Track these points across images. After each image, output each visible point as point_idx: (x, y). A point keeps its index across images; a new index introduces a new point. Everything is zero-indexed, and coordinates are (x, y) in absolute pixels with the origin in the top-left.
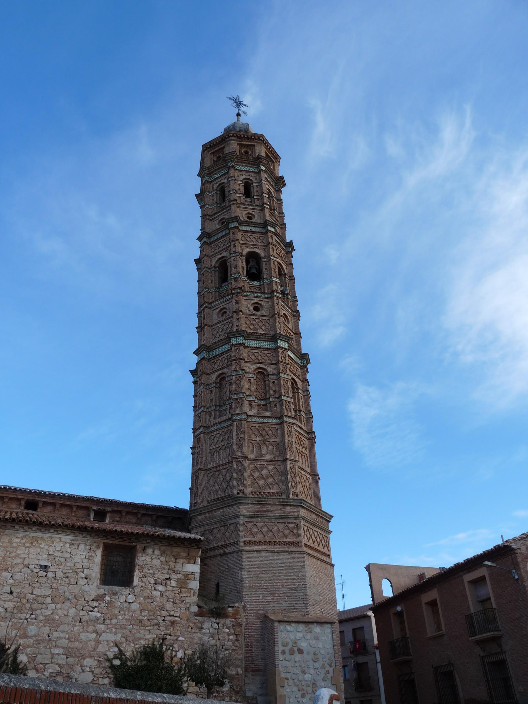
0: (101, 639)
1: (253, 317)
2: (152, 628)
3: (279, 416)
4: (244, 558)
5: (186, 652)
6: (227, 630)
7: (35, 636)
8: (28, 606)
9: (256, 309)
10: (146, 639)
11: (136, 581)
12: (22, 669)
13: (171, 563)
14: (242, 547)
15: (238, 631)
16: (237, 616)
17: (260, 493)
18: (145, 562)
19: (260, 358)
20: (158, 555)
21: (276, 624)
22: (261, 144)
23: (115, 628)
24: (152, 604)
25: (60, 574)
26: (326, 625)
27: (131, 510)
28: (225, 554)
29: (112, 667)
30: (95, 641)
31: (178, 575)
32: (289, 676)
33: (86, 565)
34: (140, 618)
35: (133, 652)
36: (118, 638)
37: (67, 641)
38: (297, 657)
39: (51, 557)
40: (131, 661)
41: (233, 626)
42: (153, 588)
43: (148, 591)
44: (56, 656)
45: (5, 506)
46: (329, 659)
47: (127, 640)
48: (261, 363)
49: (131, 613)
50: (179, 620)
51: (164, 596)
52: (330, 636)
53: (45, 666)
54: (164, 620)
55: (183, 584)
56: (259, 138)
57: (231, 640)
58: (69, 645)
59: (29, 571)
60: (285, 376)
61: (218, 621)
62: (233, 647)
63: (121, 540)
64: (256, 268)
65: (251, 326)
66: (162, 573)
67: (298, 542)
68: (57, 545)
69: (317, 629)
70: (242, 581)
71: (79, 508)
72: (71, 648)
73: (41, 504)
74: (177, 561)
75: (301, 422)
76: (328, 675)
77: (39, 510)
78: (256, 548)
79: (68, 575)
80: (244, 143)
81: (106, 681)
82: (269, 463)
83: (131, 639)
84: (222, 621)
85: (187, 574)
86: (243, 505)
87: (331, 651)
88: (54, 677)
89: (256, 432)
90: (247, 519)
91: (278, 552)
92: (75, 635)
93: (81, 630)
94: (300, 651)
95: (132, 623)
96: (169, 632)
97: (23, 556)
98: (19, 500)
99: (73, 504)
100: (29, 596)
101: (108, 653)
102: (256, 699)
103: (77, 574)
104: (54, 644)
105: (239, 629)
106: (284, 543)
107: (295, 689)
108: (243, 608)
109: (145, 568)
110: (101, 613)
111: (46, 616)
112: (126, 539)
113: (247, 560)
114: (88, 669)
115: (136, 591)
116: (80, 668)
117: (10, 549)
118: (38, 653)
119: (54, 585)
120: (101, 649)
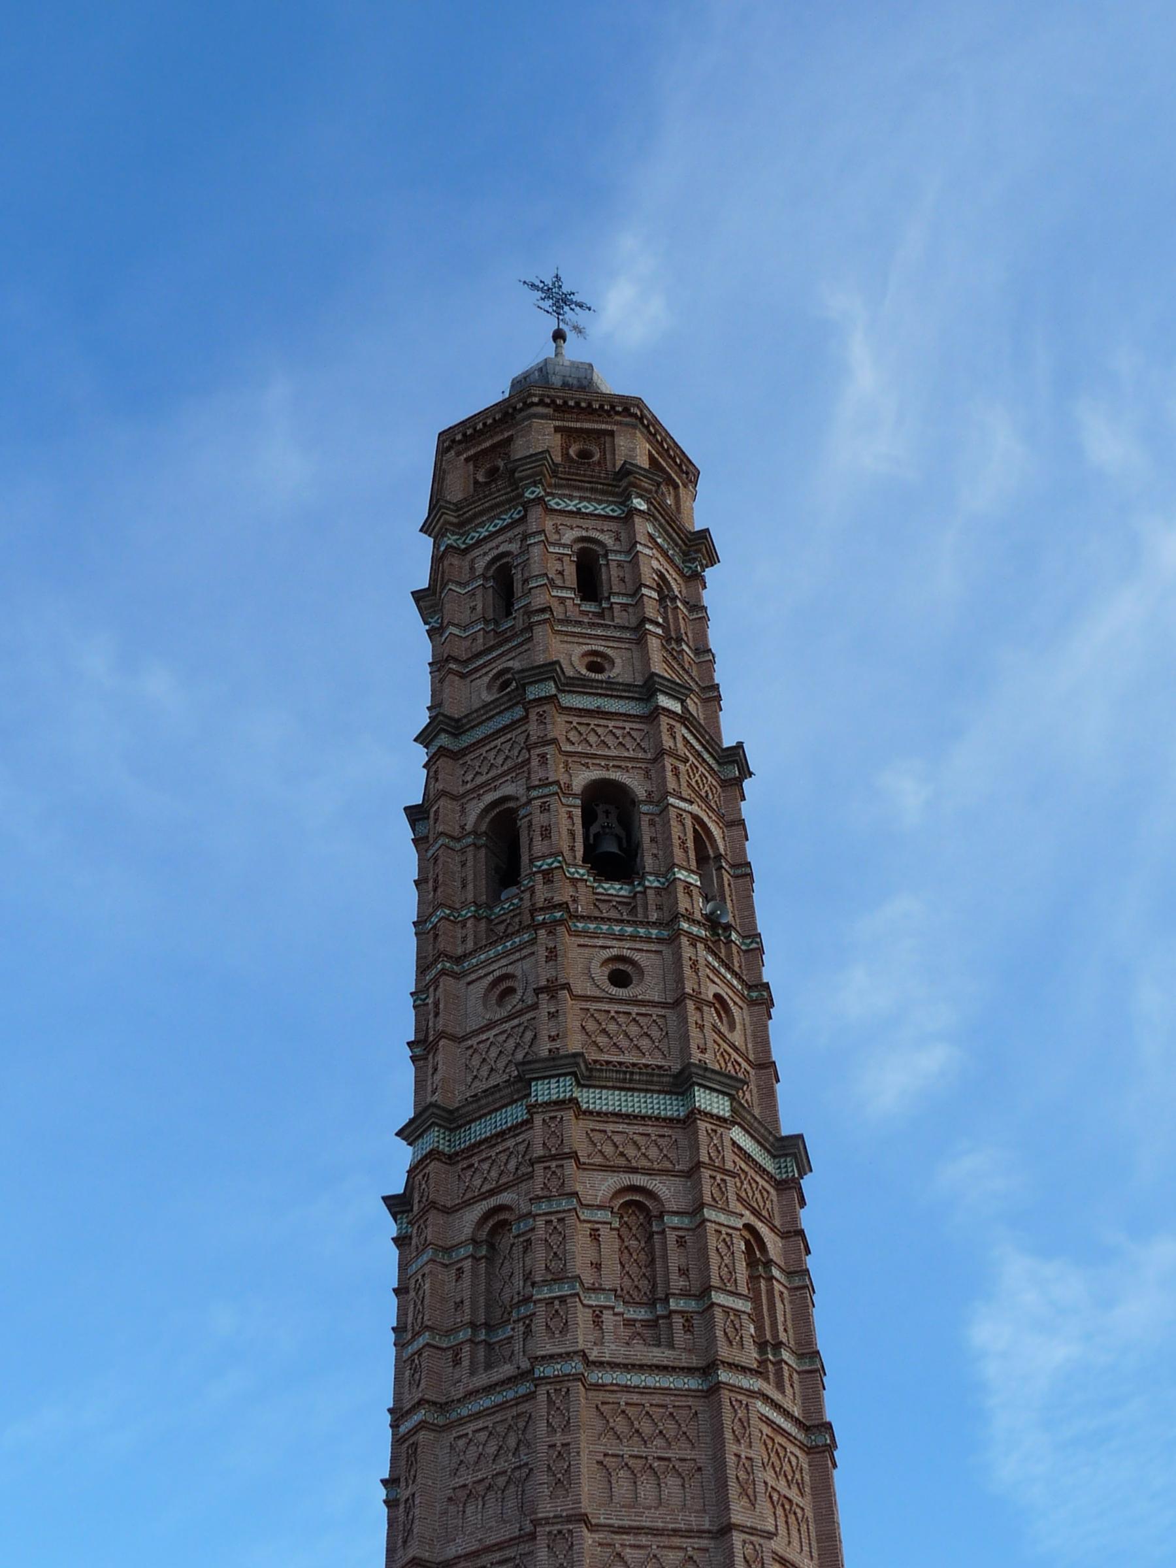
1: (606, 1007)
9: (619, 979)
19: (631, 1152)
22: (634, 427)
48: (635, 1170)
60: (722, 1218)
64: (619, 839)
65: (602, 1040)
75: (780, 1387)
80: (578, 425)
82: (665, 1541)
89: (620, 1425)
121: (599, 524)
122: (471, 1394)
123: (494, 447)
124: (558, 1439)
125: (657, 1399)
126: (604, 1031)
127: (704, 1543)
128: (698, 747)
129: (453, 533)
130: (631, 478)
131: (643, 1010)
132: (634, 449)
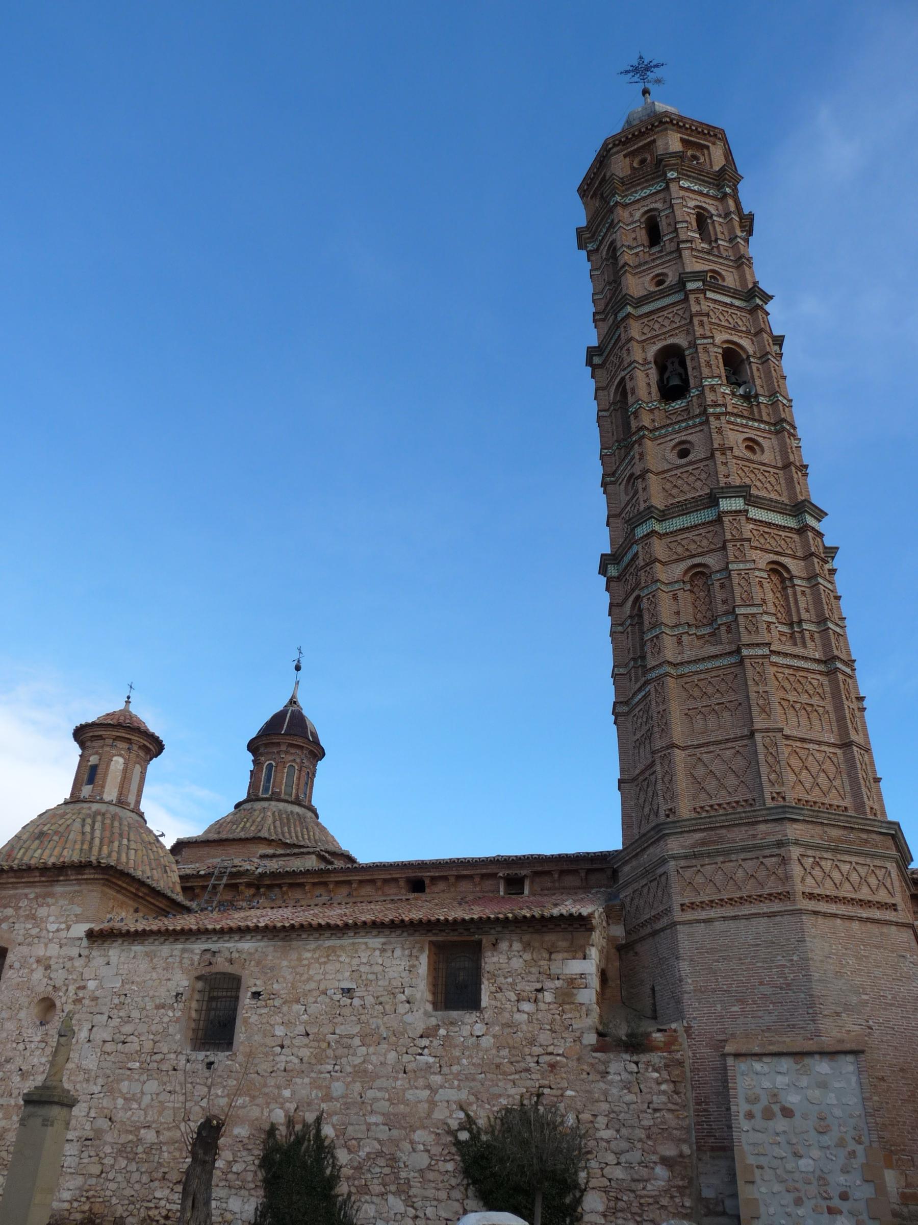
0: (437, 1098)
1: (675, 472)
2: (517, 1076)
3: (734, 648)
4: (680, 936)
5: (580, 1116)
6: (656, 1075)
7: (343, 1097)
8: (330, 1052)
9: (684, 454)
10: (509, 1096)
11: (485, 1001)
12: (329, 1147)
13: (542, 963)
14: (678, 916)
15: (678, 1076)
16: (674, 1048)
17: (711, 806)
18: (498, 966)
19: (692, 547)
20: (518, 952)
21: (730, 1061)
22: (666, 129)
23: (458, 1080)
24: (515, 1036)
25: (370, 1000)
26: (842, 1057)
27: (565, 867)
28: (655, 933)
29: (457, 1143)
30: (428, 1101)
31: (556, 982)
32: (763, 1161)
33: (406, 981)
34: (497, 1060)
35: (489, 1118)
36: (463, 1095)
37: (387, 1103)
38: (781, 1124)
39: (356, 975)
40: (486, 1133)
41: (667, 1066)
42: (515, 1009)
43: (507, 1015)
44: (373, 1127)
45: (380, 893)
46: (855, 1128)
47: (478, 1099)
48: (694, 556)
49: (481, 1054)
50: (565, 1060)
51: (534, 1021)
52: (854, 1079)
53: (359, 1143)
54: (537, 1062)
55: (566, 996)
56: (661, 122)
57: (664, 1092)
58: (391, 1110)
59: (328, 1000)
60: (741, 566)
61: (635, 1058)
62: (670, 1106)
63: (456, 933)
64: (680, 375)
65: (675, 491)
66: (529, 981)
67: (788, 892)
68: (362, 955)
69: (823, 1067)
70: (681, 981)
71: (484, 876)
72: (394, 1115)
73: (427, 882)
74: (553, 956)
75: (804, 645)
76: (852, 1160)
77: (427, 890)
78: (703, 915)
79: (381, 999)
80: (636, 147)
81: (450, 1166)
82: (723, 746)
83: (485, 1097)
84: (644, 1058)
85: (572, 979)
86: (672, 838)
87: (858, 1111)
88: (374, 1159)
89: (696, 693)
90: (683, 863)
91: (748, 917)
92: (397, 1094)
93: (407, 1086)
94: (787, 1113)
95: (484, 1070)
96: (547, 1082)
97: (317, 978)
98: (396, 880)
99: (472, 872)
100: (331, 1037)
101: (450, 1121)
102: (723, 1202)
103: (395, 997)
104: (369, 1108)
105: (677, 1072)
106: (760, 898)
107: (777, 1188)
108: (686, 1031)
109: (499, 976)
110: (435, 1057)
111: (355, 1066)
112: (462, 931)
113: (687, 940)
114: (421, 1147)
115: (486, 1016)
116: (409, 1146)
117: (300, 970)
118: (349, 1124)
119: (363, 1017)
120: (439, 1114)
121: (654, 199)
122: (635, 694)
123: (600, 183)
124: (661, 708)
125: (714, 674)
126: (675, 486)
127: (745, 742)
128: (728, 300)
129: (590, 243)
130: (663, 163)
131: (695, 466)
132: (667, 143)
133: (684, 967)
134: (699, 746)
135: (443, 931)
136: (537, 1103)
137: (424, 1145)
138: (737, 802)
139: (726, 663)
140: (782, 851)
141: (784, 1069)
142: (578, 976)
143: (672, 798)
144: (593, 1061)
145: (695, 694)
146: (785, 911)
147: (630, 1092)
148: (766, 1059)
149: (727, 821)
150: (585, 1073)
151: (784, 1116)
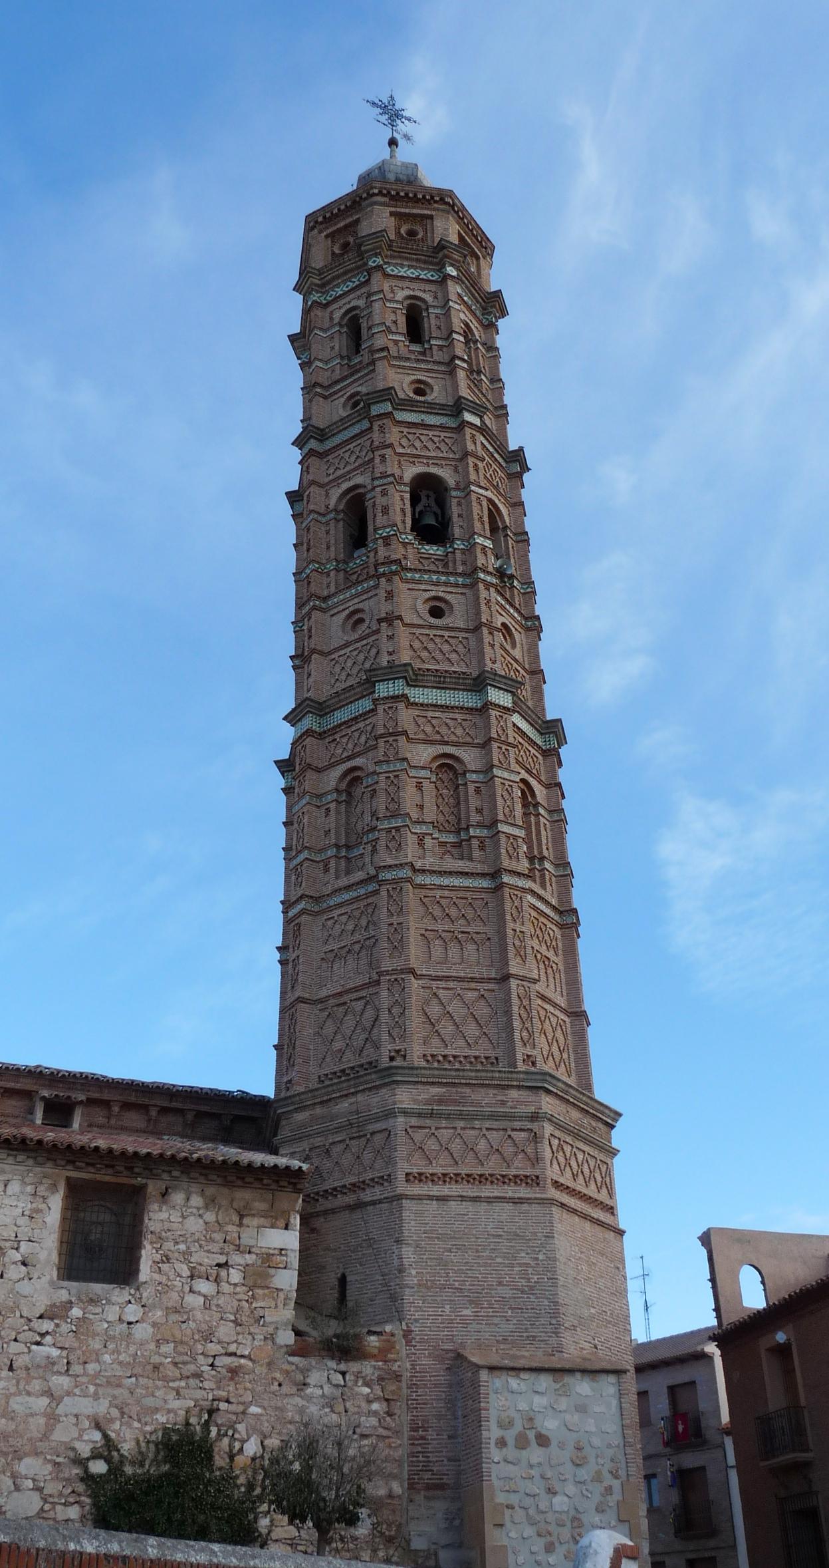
0: (60, 1410)
1: (427, 632)
2: (183, 1384)
4: (405, 1214)
5: (266, 1442)
6: (367, 1390)
9: (436, 612)
10: (169, 1411)
13: (230, 1228)
14: (402, 1187)
15: (393, 1392)
16: (390, 1356)
17: (445, 1057)
19: (444, 731)
20: (198, 1209)
21: (484, 1375)
23: (96, 1385)
24: (184, 1326)
28: (360, 1205)
30: (45, 1414)
31: (247, 1256)
32: (514, 1499)
34: (156, 1359)
35: (138, 1442)
36: (102, 1408)
38: (535, 1454)
40: (132, 1463)
41: (380, 1379)
42: (187, 1288)
43: (175, 1296)
46: (612, 1460)
47: (123, 1413)
48: (446, 743)
49: (132, 1349)
50: (250, 1364)
51: (214, 1308)
52: (614, 1402)
54: (212, 1365)
56: (442, 199)
57: (375, 1413)
60: (506, 775)
61: (343, 1367)
62: (381, 1431)
63: (110, 1171)
64: (436, 514)
65: (424, 654)
66: (208, 1251)
67: (537, 1177)
70: (400, 1271)
74: (245, 1221)
76: (609, 1497)
78: (435, 1190)
80: (407, 211)
81: (73, 1512)
82: (466, 985)
83: (134, 1410)
84: (354, 1367)
85: (269, 1255)
86: (403, 1088)
89: (437, 911)
90: (414, 1121)
91: (489, 1200)
94: (543, 1441)
95: (135, 1372)
96: (224, 1394)
101: (78, 1445)
102: (436, 1554)
106: (504, 1179)
107: (529, 1531)
108: (404, 1336)
109: (167, 1240)
113: (416, 1219)
115: (145, 1295)
116: (10, 1482)
120: (61, 1434)
123: (346, 227)
126: (426, 648)
128: (491, 450)
130: (445, 251)
133: (408, 1254)
134: (437, 978)
135: (93, 1165)
136: (207, 1422)
137: (34, 1480)
138: (476, 1058)
139: (476, 884)
140: (535, 1126)
141: (542, 1389)
142: (277, 1252)
143: (403, 1037)
144: (288, 1367)
145: (435, 913)
146: (536, 1199)
147: (333, 1411)
148: (523, 1375)
149: (476, 1078)
150: (276, 1384)
151: (540, 1445)
